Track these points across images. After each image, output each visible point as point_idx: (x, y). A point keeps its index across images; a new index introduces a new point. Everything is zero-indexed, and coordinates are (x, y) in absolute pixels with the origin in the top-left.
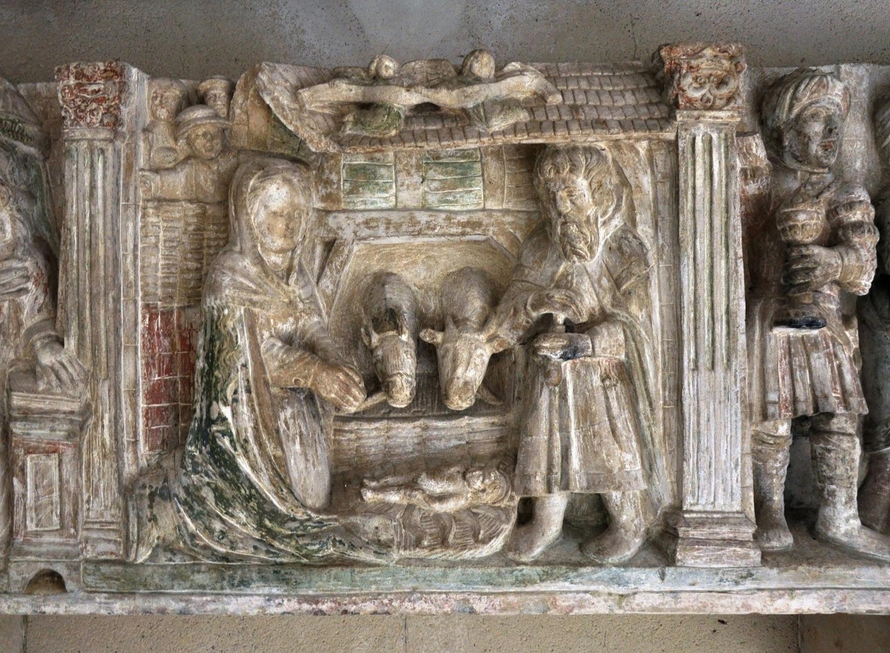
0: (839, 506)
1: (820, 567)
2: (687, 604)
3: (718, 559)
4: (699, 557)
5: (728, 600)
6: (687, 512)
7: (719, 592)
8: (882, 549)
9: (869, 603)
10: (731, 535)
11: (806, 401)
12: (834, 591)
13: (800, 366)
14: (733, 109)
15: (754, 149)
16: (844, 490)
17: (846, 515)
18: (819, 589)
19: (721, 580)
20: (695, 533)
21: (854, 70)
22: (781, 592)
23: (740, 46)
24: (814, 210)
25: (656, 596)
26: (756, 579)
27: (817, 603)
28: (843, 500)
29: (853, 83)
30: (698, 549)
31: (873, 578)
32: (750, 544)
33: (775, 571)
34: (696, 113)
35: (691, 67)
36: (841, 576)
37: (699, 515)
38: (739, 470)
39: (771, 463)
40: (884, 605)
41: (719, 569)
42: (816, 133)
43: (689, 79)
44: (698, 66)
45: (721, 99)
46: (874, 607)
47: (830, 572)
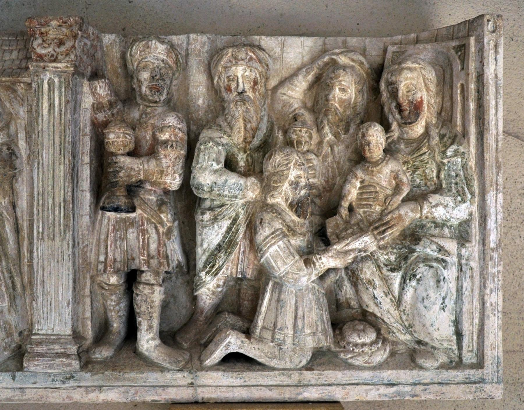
0: (143, 332)
1: (120, 372)
2: (30, 397)
3: (51, 367)
4: (37, 365)
5: (57, 393)
6: (35, 334)
7: (52, 388)
8: (165, 360)
9: (154, 395)
10: (62, 350)
11: (121, 262)
12: (129, 388)
13: (120, 238)
14: (68, 61)
15: (98, 89)
16: (146, 321)
17: (147, 338)
18: (119, 386)
19: (53, 381)
20: (39, 349)
21: (199, 38)
22: (93, 388)
23: (77, 19)
24: (121, 131)
25: (9, 391)
26: (76, 380)
27: (117, 395)
28: (146, 328)
29: (199, 47)
30: (37, 360)
31: (157, 379)
32: (73, 357)
33: (89, 374)
34: (42, 64)
35: (42, 33)
36: (134, 378)
37: (41, 337)
38: (70, 308)
39: (109, 302)
40: (163, 397)
41: (52, 373)
42: (145, 79)
43: (40, 41)
44: (47, 32)
45: (62, 55)
46: (156, 398)
47: (126, 376)
